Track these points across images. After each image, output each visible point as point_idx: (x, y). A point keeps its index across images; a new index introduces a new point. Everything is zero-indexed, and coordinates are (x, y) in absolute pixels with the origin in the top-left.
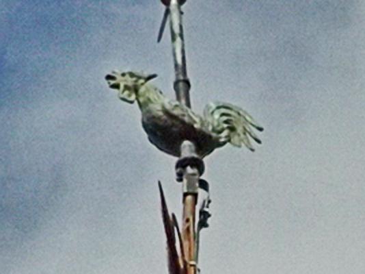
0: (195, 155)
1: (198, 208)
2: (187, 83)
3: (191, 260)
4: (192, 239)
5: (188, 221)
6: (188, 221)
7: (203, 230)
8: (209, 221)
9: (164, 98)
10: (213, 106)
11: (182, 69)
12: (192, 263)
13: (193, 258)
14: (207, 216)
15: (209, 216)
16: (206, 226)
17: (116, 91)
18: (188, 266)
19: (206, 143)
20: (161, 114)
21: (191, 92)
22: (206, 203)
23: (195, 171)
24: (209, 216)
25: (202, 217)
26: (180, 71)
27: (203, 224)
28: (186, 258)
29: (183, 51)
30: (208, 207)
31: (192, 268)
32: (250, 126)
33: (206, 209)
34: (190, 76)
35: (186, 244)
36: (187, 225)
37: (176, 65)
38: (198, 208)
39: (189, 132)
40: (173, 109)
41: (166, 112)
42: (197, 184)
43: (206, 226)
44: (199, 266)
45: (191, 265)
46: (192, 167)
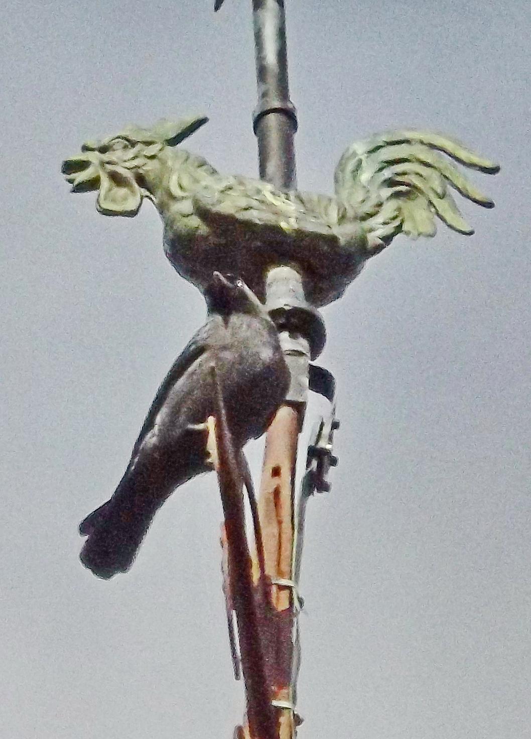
0: (303, 304)
1: (305, 441)
2: (289, 115)
3: (280, 573)
4: (287, 524)
5: (276, 472)
6: (276, 472)
7: (317, 497)
8: (331, 475)
9: (229, 178)
10: (360, 148)
11: (276, 77)
12: (284, 582)
13: (284, 567)
14: (326, 460)
15: (334, 462)
16: (323, 487)
17: (91, 195)
18: (274, 589)
19: (328, 264)
20: (195, 222)
21: (297, 137)
22: (326, 430)
23: (302, 344)
24: (334, 462)
25: (314, 464)
26: (272, 82)
27: (315, 482)
28: (270, 570)
29: (281, 34)
30: (330, 439)
31: (285, 594)
32: (113, 141)
33: (323, 444)
34: (295, 100)
35: (269, 531)
36: (276, 481)
37: (262, 72)
38: (305, 441)
39: (275, 246)
40: (399, 209)
41: (203, 213)
42: (306, 381)
43: (323, 487)
44: (300, 591)
45: (281, 588)
46: (293, 336)
